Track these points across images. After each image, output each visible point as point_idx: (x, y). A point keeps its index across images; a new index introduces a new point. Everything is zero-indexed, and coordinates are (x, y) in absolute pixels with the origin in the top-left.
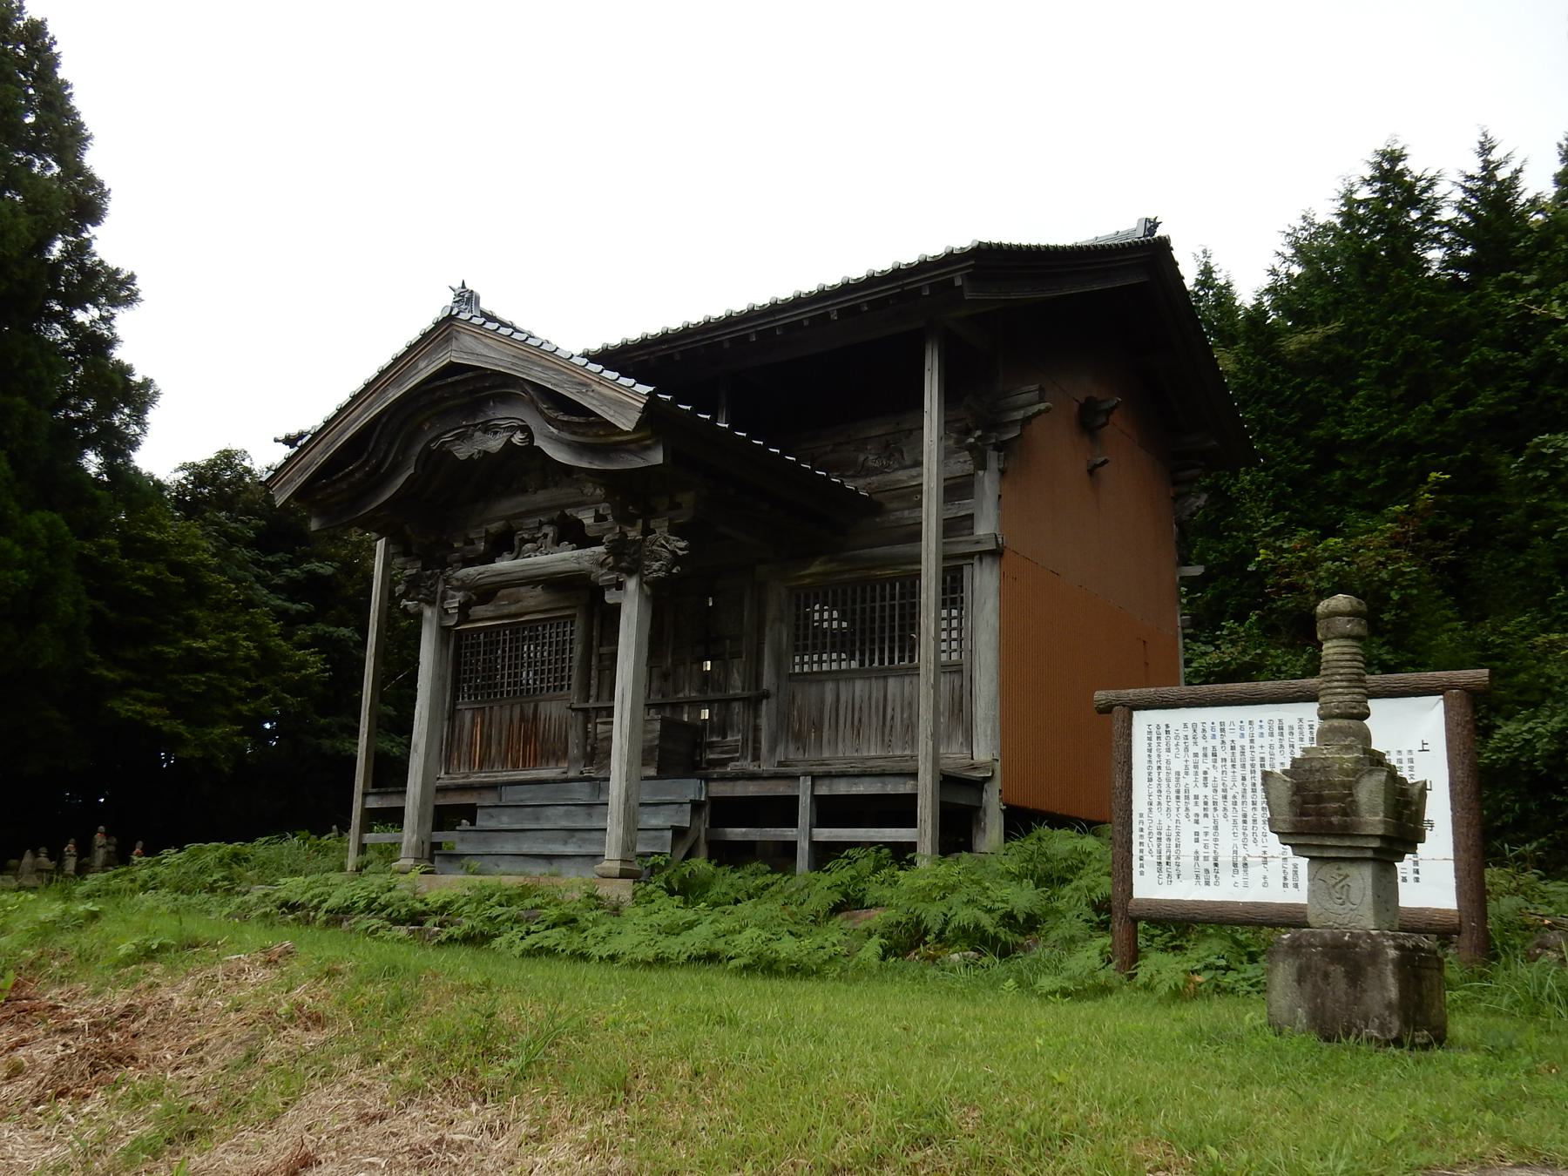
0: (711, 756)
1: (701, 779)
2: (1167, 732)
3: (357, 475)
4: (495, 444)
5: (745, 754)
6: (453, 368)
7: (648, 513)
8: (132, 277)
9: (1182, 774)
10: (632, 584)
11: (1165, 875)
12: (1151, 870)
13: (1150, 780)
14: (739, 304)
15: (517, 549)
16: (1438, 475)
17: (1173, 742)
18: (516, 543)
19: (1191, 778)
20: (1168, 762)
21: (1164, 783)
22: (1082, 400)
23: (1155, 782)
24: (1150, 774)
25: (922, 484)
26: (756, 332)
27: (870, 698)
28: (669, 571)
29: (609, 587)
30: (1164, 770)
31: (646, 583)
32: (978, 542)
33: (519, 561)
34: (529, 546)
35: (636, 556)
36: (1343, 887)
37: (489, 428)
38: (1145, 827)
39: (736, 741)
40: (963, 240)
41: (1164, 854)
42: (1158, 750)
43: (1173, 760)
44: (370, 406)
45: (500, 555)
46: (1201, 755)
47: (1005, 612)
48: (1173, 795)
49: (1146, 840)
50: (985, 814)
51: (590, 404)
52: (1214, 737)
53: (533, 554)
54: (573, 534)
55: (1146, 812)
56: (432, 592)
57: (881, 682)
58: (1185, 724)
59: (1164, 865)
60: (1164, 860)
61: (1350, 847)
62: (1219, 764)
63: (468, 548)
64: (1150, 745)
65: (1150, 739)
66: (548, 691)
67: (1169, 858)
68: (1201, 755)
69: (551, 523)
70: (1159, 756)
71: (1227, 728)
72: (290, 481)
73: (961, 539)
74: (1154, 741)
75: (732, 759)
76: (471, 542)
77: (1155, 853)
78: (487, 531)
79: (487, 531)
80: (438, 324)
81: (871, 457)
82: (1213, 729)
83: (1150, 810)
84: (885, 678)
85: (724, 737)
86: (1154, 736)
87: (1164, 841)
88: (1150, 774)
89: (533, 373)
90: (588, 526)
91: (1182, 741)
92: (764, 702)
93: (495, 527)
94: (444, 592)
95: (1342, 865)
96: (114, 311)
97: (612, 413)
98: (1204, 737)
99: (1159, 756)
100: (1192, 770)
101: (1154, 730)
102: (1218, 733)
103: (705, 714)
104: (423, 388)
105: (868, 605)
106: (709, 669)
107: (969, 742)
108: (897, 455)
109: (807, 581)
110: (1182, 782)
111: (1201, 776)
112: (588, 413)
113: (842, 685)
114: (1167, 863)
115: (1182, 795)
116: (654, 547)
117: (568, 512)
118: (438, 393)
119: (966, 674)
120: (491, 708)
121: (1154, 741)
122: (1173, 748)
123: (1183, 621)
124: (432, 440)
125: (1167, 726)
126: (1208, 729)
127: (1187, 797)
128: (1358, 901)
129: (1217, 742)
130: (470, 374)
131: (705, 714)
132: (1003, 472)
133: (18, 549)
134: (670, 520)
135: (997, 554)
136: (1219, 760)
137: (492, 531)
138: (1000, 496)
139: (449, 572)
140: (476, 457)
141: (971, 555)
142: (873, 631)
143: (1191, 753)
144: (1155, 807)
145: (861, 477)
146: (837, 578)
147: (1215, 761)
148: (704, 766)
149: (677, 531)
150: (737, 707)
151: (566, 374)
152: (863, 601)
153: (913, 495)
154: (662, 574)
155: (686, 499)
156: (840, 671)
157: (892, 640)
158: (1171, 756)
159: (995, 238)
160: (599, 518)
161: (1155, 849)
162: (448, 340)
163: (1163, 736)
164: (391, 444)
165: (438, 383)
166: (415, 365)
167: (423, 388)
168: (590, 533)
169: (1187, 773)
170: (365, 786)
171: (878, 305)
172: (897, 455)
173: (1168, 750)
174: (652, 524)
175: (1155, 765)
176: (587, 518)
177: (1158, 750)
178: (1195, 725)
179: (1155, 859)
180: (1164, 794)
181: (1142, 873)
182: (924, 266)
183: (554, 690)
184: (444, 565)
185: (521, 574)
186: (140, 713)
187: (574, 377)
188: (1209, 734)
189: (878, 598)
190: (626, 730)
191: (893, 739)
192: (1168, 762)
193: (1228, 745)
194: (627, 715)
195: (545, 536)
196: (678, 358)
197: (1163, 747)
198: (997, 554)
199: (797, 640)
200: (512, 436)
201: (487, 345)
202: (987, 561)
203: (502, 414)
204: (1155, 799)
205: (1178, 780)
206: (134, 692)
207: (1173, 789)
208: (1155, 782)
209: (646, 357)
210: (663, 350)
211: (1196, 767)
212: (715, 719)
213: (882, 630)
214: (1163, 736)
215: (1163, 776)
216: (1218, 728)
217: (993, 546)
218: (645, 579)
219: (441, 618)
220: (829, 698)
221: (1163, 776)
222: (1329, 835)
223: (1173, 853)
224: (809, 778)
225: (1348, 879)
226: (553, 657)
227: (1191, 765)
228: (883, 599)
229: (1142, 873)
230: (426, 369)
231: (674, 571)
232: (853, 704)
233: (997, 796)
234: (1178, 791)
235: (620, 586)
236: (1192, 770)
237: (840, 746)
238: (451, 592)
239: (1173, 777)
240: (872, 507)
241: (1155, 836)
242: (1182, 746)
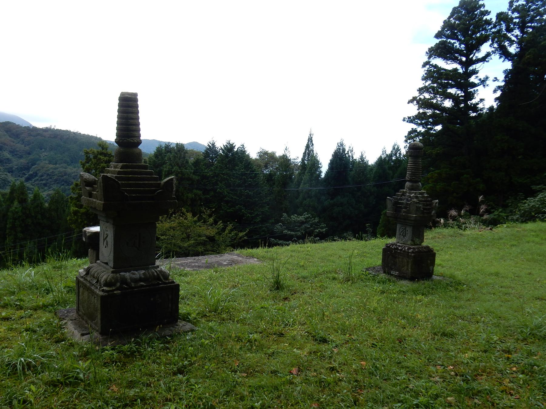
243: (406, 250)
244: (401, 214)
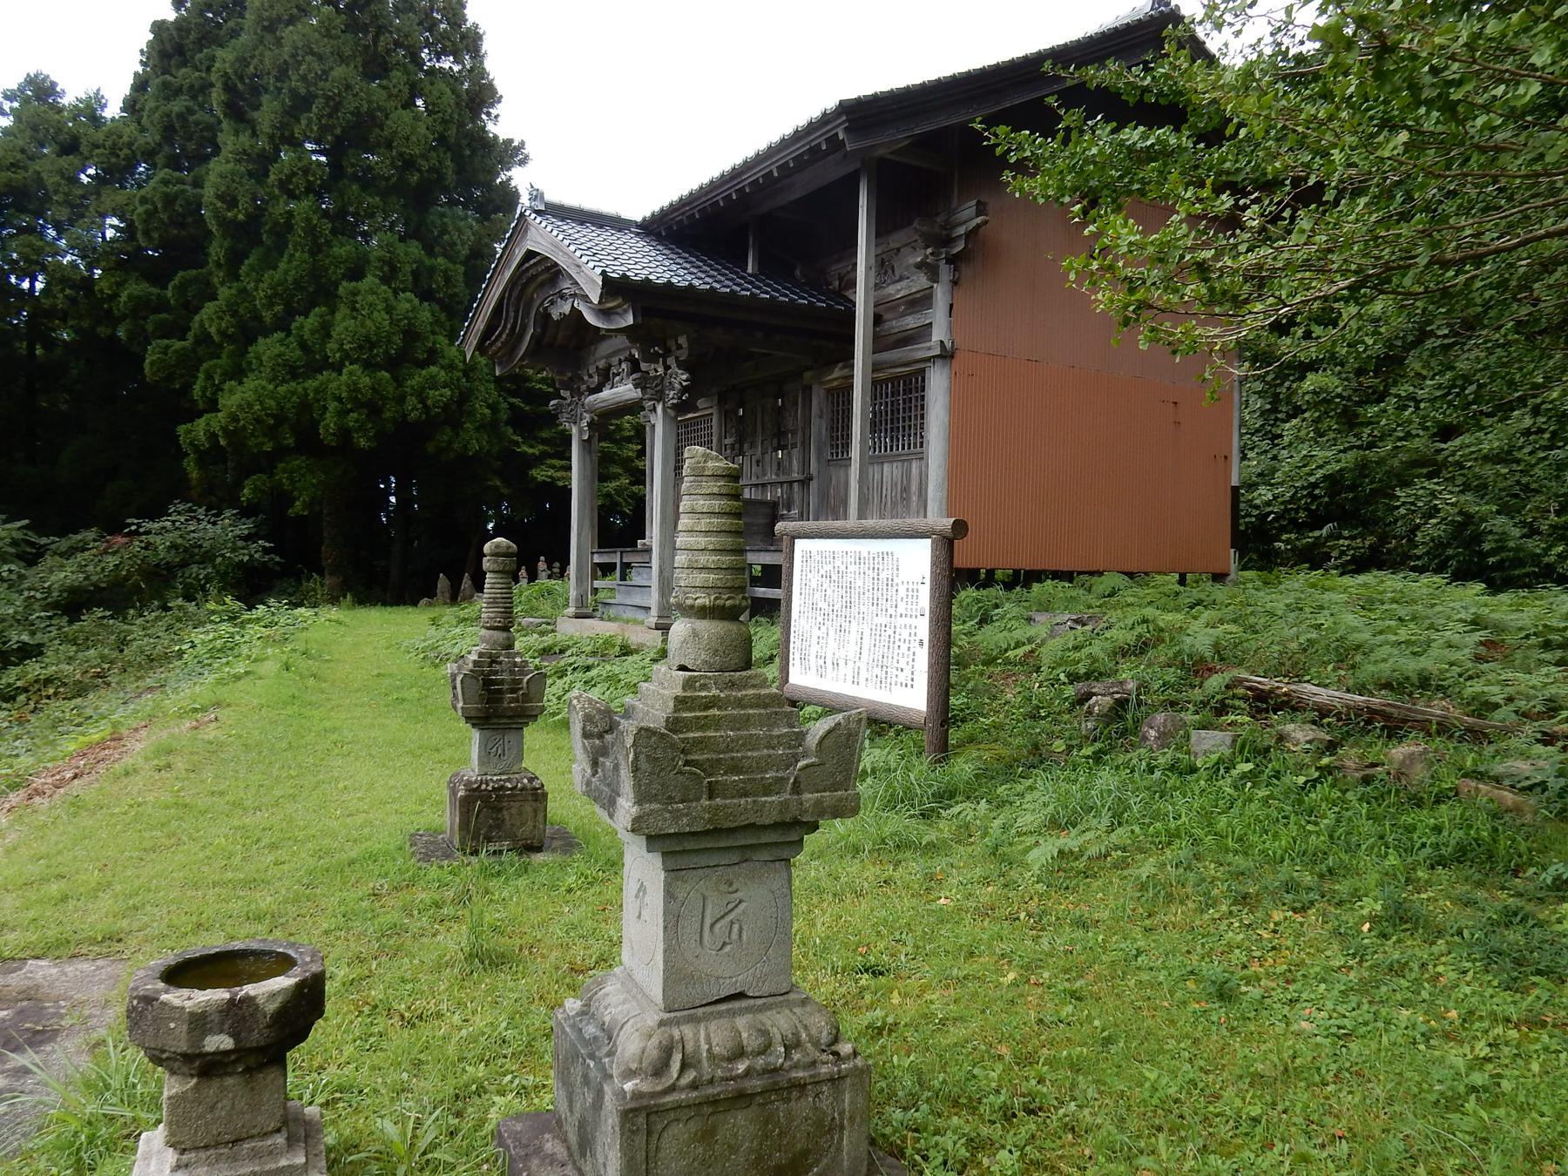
8: (523, 143)
14: (738, 160)
16: (525, 448)
28: (680, 398)
34: (617, 378)
40: (831, 103)
96: (508, 174)
109: (835, 383)
132: (955, 283)
133: (443, 373)
135: (947, 355)
138: (951, 306)
141: (928, 360)
150: (796, 485)
159: (852, 94)
186: (551, 477)
198: (947, 355)
202: (939, 363)
206: (549, 461)
217: (937, 352)
243: (529, 786)
244: (505, 705)
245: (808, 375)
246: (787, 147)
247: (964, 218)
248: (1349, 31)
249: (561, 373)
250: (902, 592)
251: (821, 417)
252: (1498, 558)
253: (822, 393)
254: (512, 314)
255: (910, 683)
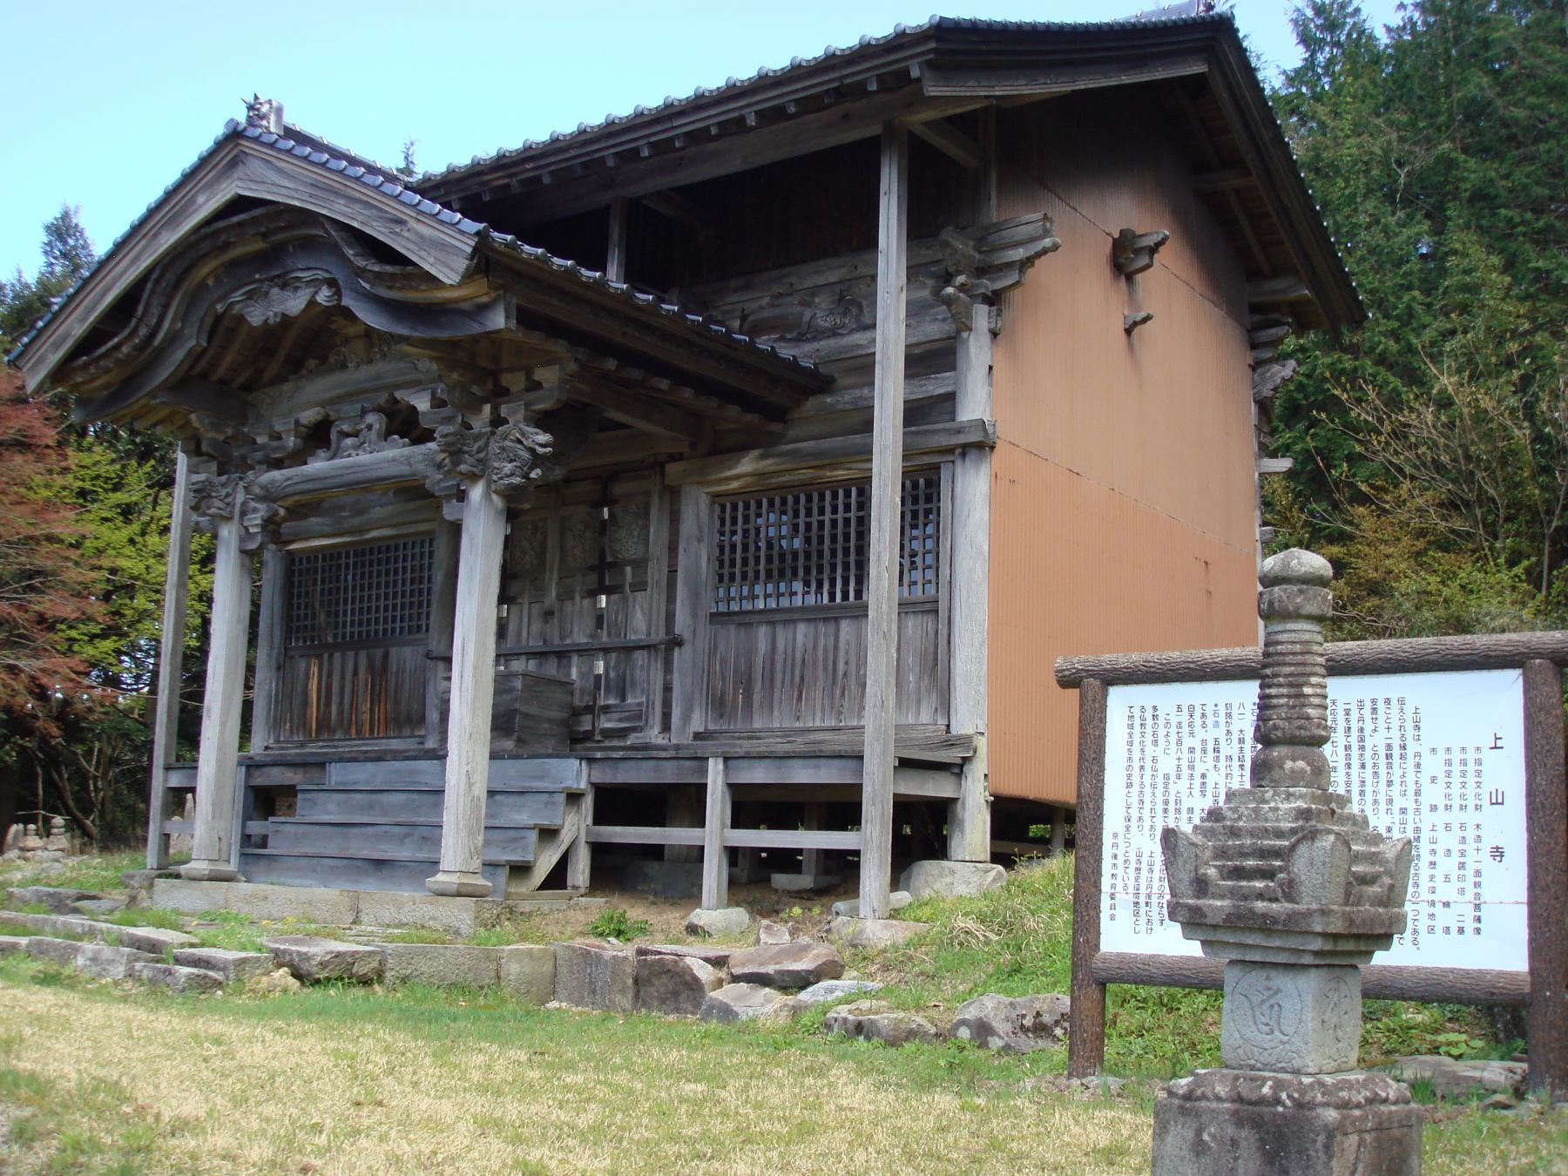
0: (608, 725)
1: (581, 759)
2: (1155, 717)
3: (125, 349)
4: (295, 304)
5: (650, 721)
6: (240, 204)
7: (499, 394)
9: (1173, 777)
10: (477, 492)
11: (1143, 919)
12: (1124, 914)
13: (1129, 785)
15: (334, 446)
17: (1162, 731)
18: (333, 436)
19: (1183, 784)
20: (1154, 759)
21: (1148, 790)
22: (1116, 235)
23: (1136, 789)
24: (1129, 776)
25: (874, 354)
26: (649, 143)
27: (815, 647)
29: (448, 497)
30: (1148, 772)
31: (496, 492)
32: (959, 431)
33: (337, 462)
34: (349, 441)
35: (481, 455)
36: (1272, 1006)
37: (286, 284)
38: (1121, 852)
39: (640, 704)
40: (917, 17)
41: (1143, 890)
42: (1142, 743)
43: (1161, 758)
44: (137, 258)
45: (312, 454)
46: (1198, 751)
47: (994, 531)
48: (1159, 807)
49: (1120, 872)
50: (964, 809)
51: (404, 247)
52: (1216, 724)
53: (354, 453)
54: (405, 425)
55: (1121, 831)
56: (228, 504)
57: (831, 627)
58: (1179, 707)
59: (1142, 905)
60: (1142, 899)
61: (1279, 948)
62: (1222, 763)
63: (275, 444)
64: (1131, 735)
65: (1131, 726)
66: (401, 633)
67: (1149, 896)
68: (1198, 751)
69: (379, 410)
70: (1142, 751)
71: (1235, 712)
72: (40, 361)
73: (939, 426)
74: (1137, 730)
75: (633, 729)
76: (277, 437)
77: (1131, 890)
78: (297, 423)
79: (297, 423)
80: (220, 145)
81: (820, 314)
82: (1215, 713)
83: (1128, 828)
84: (836, 620)
85: (623, 699)
86: (1137, 722)
87: (1144, 874)
88: (1129, 776)
89: (336, 207)
90: (424, 413)
91: (1173, 730)
92: (676, 651)
93: (309, 416)
94: (244, 504)
95: (1273, 973)
97: (432, 260)
98: (1204, 725)
99: (1142, 751)
100: (1185, 772)
101: (1137, 713)
102: (1222, 719)
103: (600, 667)
104: (203, 231)
105: (815, 519)
106: (604, 605)
107: (945, 704)
108: (854, 311)
109: (735, 485)
110: (1173, 789)
111: (1197, 781)
112: (406, 261)
113: (780, 631)
114: (1147, 904)
115: (1172, 807)
116: (507, 443)
117: (399, 395)
118: (223, 237)
119: (943, 613)
120: (331, 656)
121: (1137, 730)
122: (1161, 739)
123: (1262, 533)
124: (219, 301)
125: (1155, 708)
126: (1209, 713)
127: (1178, 811)
128: (1290, 1030)
129: (1220, 733)
130: (258, 212)
131: (600, 667)
132: (994, 334)
134: (527, 405)
136: (1222, 758)
137: (304, 421)
138: (991, 368)
139: (250, 475)
140: (271, 322)
141: (950, 450)
142: (820, 554)
143: (1185, 748)
144: (1134, 823)
145: (808, 340)
146: (774, 481)
147: (1217, 759)
148: (598, 737)
149: (542, 421)
151: (375, 207)
152: (809, 513)
153: (864, 367)
154: (517, 480)
155: (548, 376)
156: (778, 610)
157: (846, 567)
158: (1159, 751)
159: (951, 14)
160: (438, 403)
161: (1131, 884)
162: (234, 163)
163: (1149, 722)
164: (166, 307)
165: (221, 224)
166: (193, 200)
167: (203, 231)
168: (425, 424)
169: (1179, 777)
170: (167, 755)
171: (810, 104)
172: (854, 311)
173: (1155, 743)
174: (504, 411)
175: (1136, 764)
176: (422, 403)
177: (1142, 743)
178: (1191, 708)
179: (1131, 898)
180: (1147, 806)
181: (1113, 918)
182: (866, 52)
183: (409, 633)
184: (245, 466)
185: (337, 480)
187: (386, 212)
188: (1210, 721)
189: (828, 509)
190: (469, 696)
191: (846, 704)
192: (1154, 759)
193: (1235, 738)
194: (469, 674)
195: (370, 427)
196: (547, 180)
197: (1149, 738)
199: (721, 566)
200: (316, 293)
201: (280, 171)
203: (306, 269)
204: (1134, 813)
205: (1166, 785)
207: (1160, 799)
208: (1136, 789)
209: (506, 181)
210: (528, 170)
211: (1192, 767)
212: (612, 674)
213: (834, 553)
214: (1149, 722)
215: (1147, 780)
216: (1222, 711)
218: (493, 487)
219: (242, 540)
220: (762, 646)
221: (1147, 780)
222: (1251, 930)
223: (1155, 890)
224: (720, 761)
225: (1279, 996)
226: (408, 588)
227: (1184, 764)
228: (835, 510)
229: (1113, 918)
230: (208, 204)
231: (533, 475)
232: (793, 660)
233: (981, 784)
234: (1166, 802)
235: (462, 496)
236: (1185, 772)
237: (776, 713)
238: (253, 504)
239: (1160, 781)
240: (819, 382)
241: (1133, 866)
242: (1173, 738)
245: (673, 469)
246: (799, 79)
247: (1018, 238)
248: (71, 242)
249: (215, 427)
250: (1433, 765)
251: (699, 541)
252: (1252, 884)
253: (704, 501)
254: (156, 311)
255: (1470, 926)
